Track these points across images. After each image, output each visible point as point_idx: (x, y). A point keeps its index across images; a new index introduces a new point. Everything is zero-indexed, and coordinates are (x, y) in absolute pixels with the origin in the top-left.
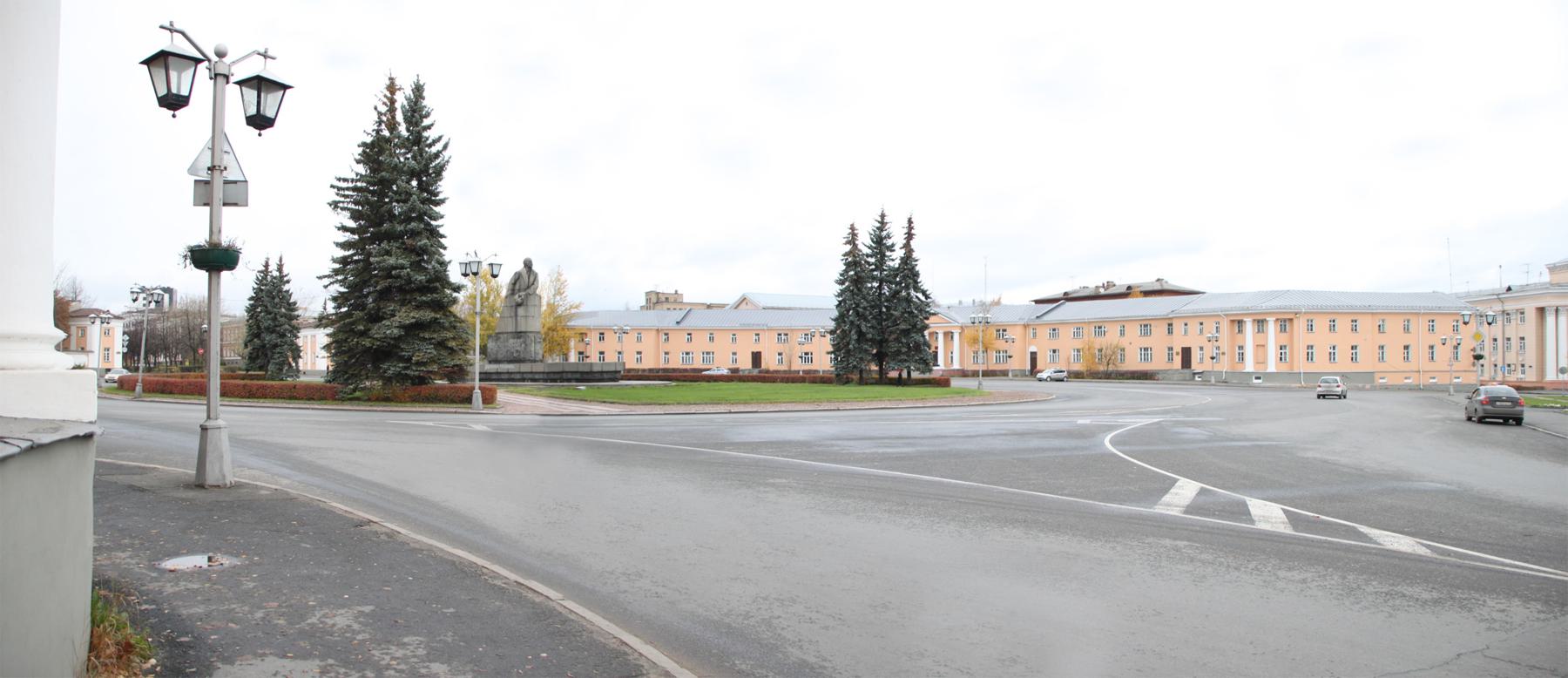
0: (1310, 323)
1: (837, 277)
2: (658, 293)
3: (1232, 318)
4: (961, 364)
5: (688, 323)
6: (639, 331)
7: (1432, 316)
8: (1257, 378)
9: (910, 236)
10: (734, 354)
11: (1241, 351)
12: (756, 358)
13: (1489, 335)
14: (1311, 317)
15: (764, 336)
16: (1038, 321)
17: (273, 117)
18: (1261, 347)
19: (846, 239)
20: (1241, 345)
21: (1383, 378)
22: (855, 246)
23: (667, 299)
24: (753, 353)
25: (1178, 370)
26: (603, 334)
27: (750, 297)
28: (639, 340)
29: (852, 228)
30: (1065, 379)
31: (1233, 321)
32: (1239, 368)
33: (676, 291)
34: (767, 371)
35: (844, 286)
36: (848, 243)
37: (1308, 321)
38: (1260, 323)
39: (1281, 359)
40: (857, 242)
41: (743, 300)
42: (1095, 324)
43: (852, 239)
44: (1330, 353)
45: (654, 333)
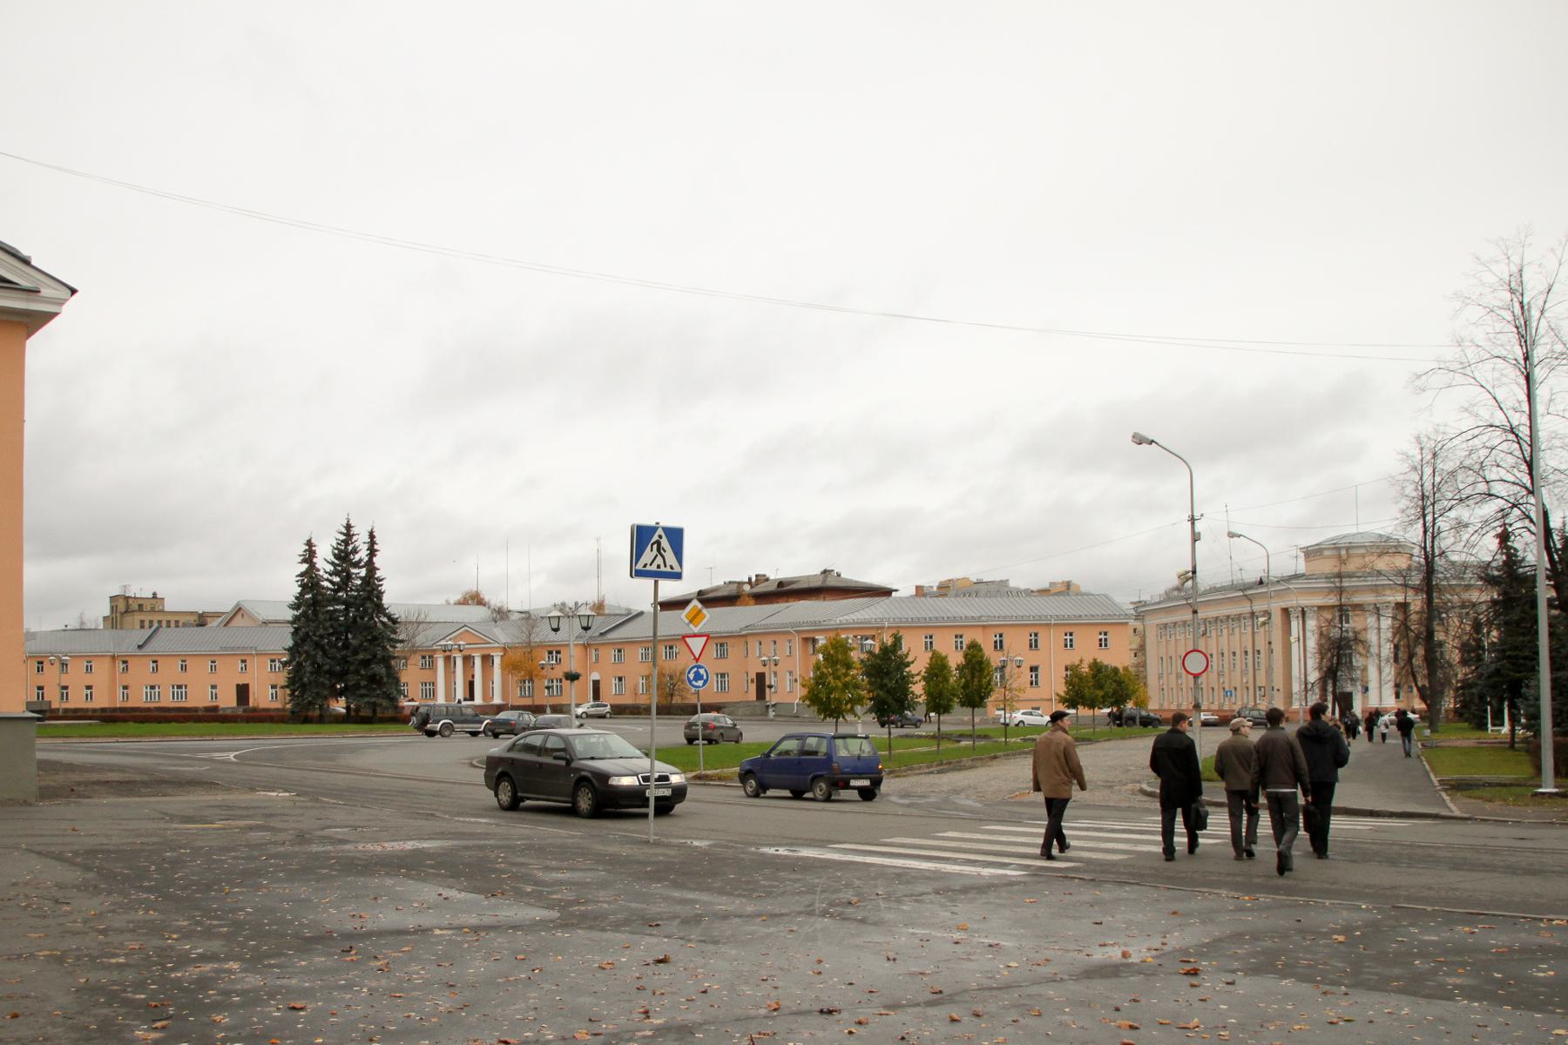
0: (928, 640)
1: (292, 600)
2: (127, 598)
3: (805, 636)
4: (503, 699)
5: (155, 647)
6: (88, 659)
9: (372, 552)
10: (214, 687)
12: (243, 692)
13: (1241, 648)
15: (254, 663)
16: (601, 640)
19: (302, 558)
22: (312, 566)
23: (140, 606)
24: (238, 686)
25: (753, 701)
26: (42, 663)
27: (246, 606)
28: (89, 669)
29: (309, 543)
30: (608, 715)
31: (806, 640)
33: (154, 594)
34: (255, 710)
35: (300, 611)
36: (304, 561)
40: (315, 560)
41: (239, 610)
42: (717, 641)
43: (309, 556)
45: (108, 660)
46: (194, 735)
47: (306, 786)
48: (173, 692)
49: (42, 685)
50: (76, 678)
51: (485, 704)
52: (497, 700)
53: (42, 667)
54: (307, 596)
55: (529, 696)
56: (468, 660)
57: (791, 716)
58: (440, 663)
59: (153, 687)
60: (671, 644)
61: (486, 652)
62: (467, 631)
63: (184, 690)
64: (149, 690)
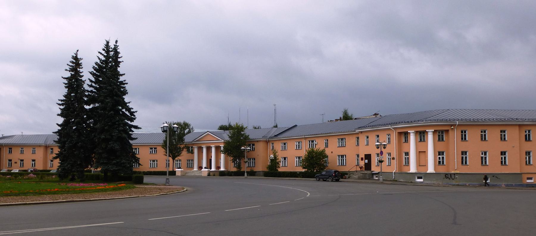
7: (34, 147)
11: (407, 157)
14: (463, 129)
18: (422, 153)
20: (407, 151)
21: (531, 179)
31: (400, 133)
32: (405, 169)
36: (71, 70)
38: (422, 135)
39: (439, 162)
44: (482, 158)
46: (25, 194)
48: (151, 163)
49: (11, 159)
50: (28, 156)
51: (217, 170)
52: (222, 169)
53: (11, 151)
54: (72, 95)
56: (209, 149)
57: (391, 181)
58: (196, 151)
60: (312, 139)
61: (217, 145)
63: (179, 162)
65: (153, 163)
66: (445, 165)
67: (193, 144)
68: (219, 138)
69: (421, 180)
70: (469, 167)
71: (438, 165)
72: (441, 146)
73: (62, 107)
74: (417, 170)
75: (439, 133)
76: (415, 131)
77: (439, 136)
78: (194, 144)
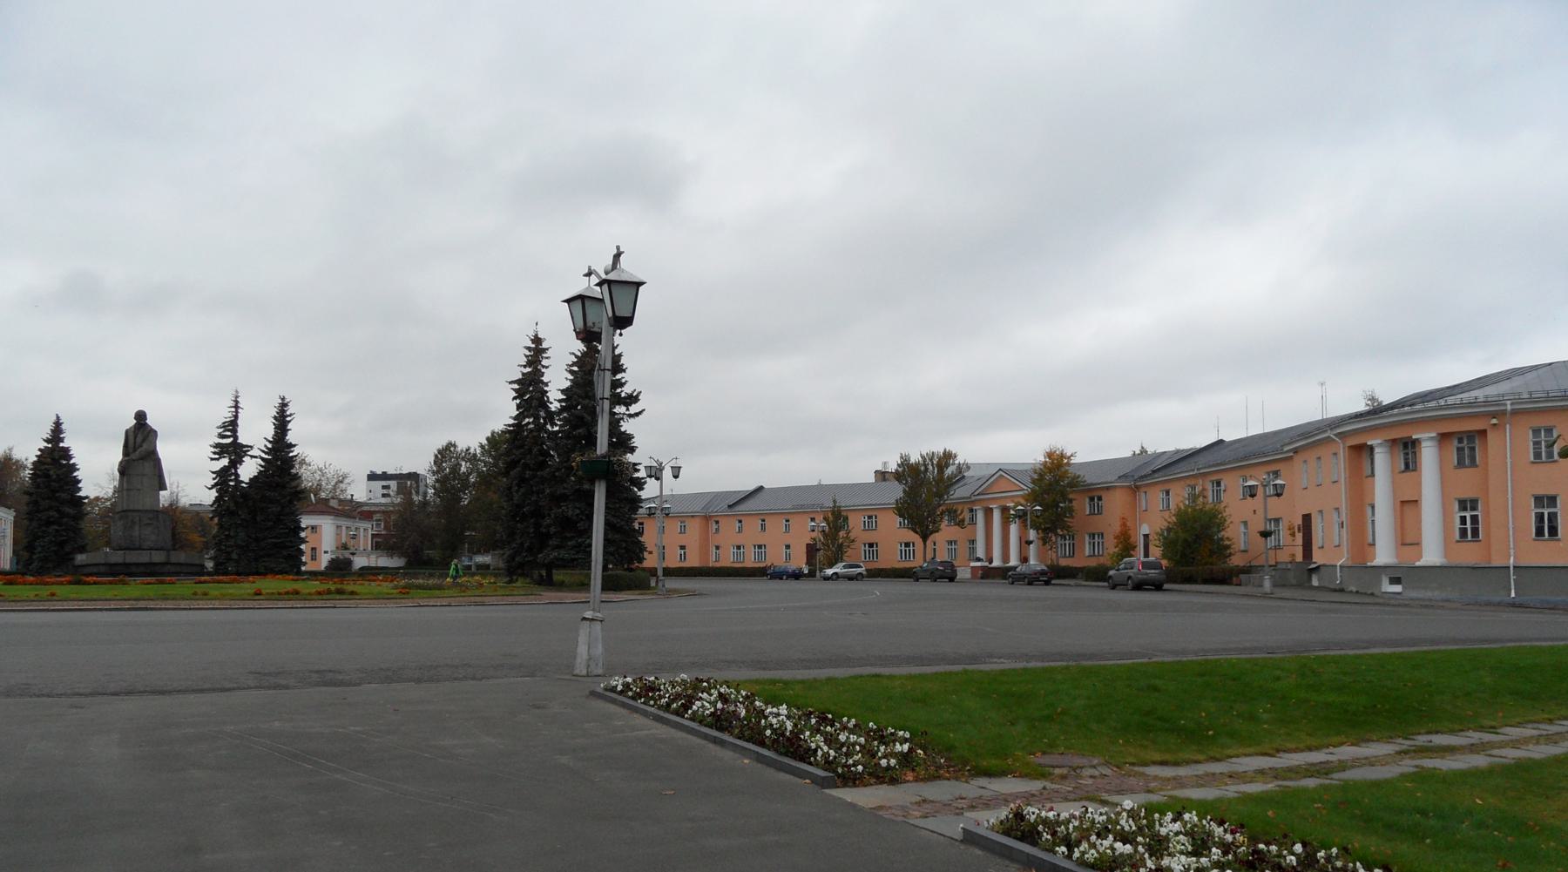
7: (683, 518)
8: (1395, 581)
17: (630, 315)
18: (1407, 506)
37: (1536, 432)
39: (1463, 533)
47: (1510, 641)
48: (901, 550)
55: (1099, 555)
56: (988, 512)
58: (980, 517)
59: (739, 548)
62: (1001, 476)
63: (875, 548)
64: (735, 550)
65: (905, 550)
66: (1480, 541)
67: (970, 503)
68: (1022, 486)
69: (1397, 588)
70: (1561, 544)
71: (1535, 540)
72: (1467, 480)
73: (262, 469)
74: (1446, 557)
75: (1460, 441)
76: (1439, 434)
77: (1460, 450)
78: (973, 502)
